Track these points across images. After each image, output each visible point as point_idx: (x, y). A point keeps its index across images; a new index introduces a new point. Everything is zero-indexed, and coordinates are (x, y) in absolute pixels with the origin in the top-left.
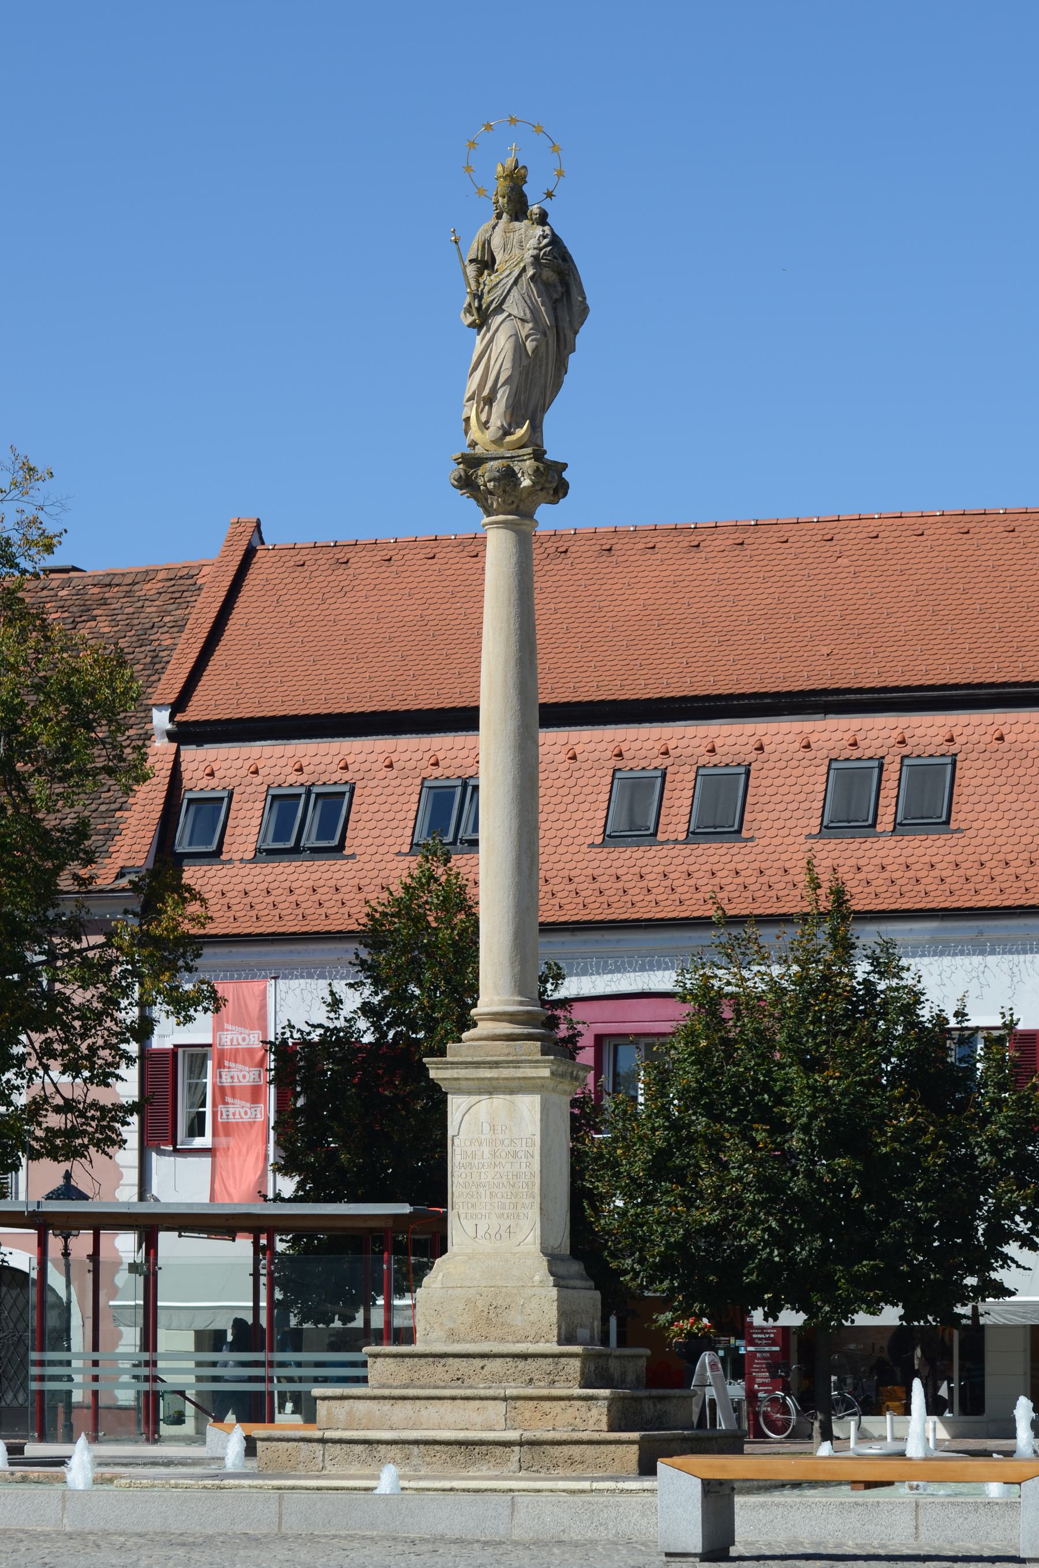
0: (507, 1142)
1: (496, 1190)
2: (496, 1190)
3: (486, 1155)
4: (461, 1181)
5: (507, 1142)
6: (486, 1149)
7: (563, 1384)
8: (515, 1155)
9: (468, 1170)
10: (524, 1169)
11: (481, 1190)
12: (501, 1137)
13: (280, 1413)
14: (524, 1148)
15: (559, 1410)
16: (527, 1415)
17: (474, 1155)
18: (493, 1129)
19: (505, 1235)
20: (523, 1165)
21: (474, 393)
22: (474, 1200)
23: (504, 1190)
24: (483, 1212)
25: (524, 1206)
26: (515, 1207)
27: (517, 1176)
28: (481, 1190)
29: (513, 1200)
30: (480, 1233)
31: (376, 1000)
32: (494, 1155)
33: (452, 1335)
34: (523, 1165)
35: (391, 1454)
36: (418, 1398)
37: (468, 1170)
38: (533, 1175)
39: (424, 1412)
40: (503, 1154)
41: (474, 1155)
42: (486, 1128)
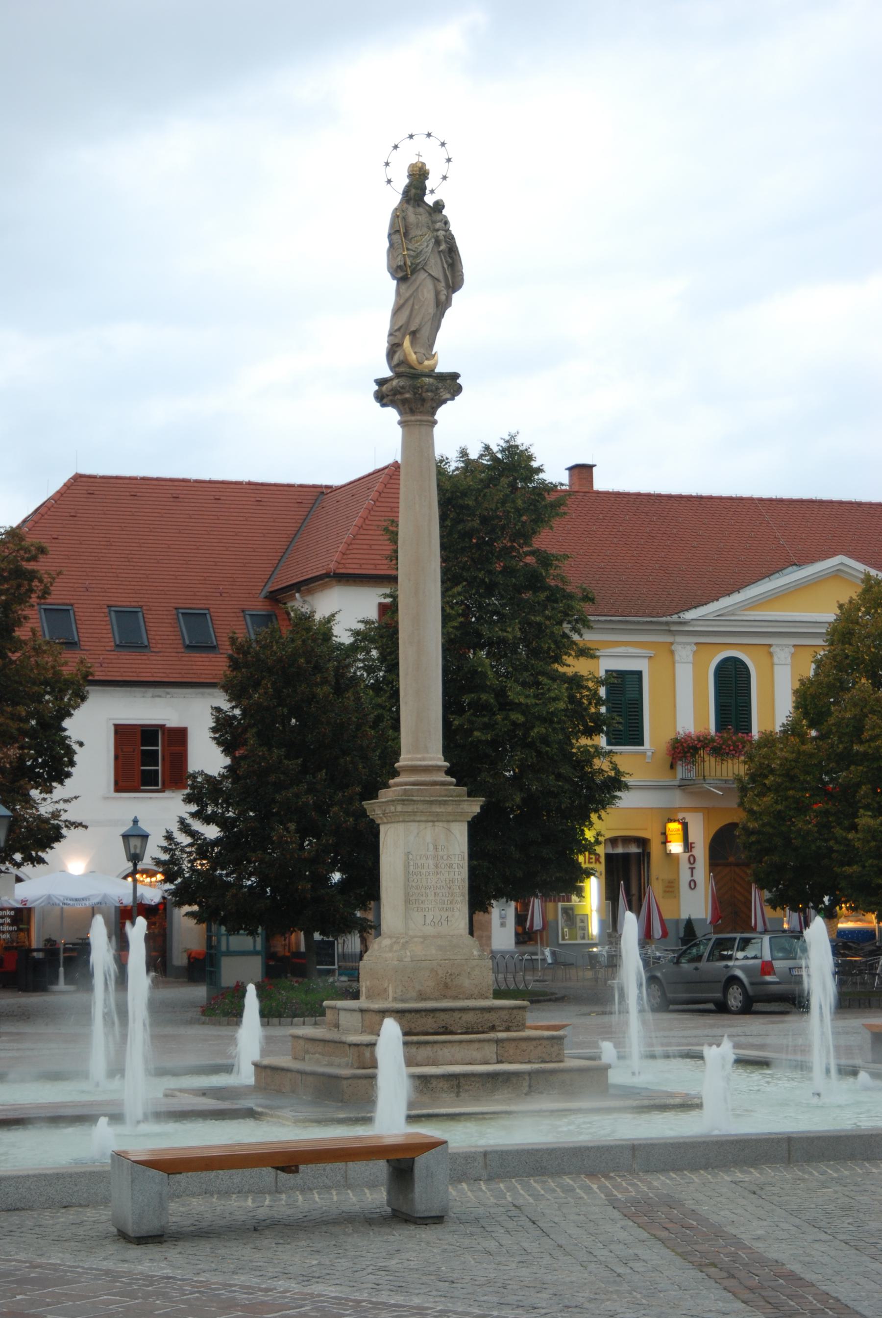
0: (445, 857)
1: (438, 891)
2: (438, 891)
3: (432, 866)
4: (414, 884)
5: (445, 857)
6: (431, 862)
7: (515, 1029)
8: (451, 866)
9: (419, 877)
10: (456, 876)
11: (428, 891)
12: (441, 853)
13: (600, 1058)
14: (457, 861)
15: (532, 1048)
16: (511, 1052)
17: (423, 866)
18: (436, 848)
19: (445, 923)
20: (456, 873)
21: (401, 327)
22: (423, 898)
23: (443, 891)
24: (430, 906)
25: (456, 902)
26: (451, 903)
27: (452, 881)
28: (428, 891)
29: (450, 898)
30: (428, 921)
31: (602, 741)
32: (437, 867)
33: (422, 996)
34: (456, 873)
35: (441, 1085)
36: (435, 1042)
37: (419, 877)
38: (463, 880)
39: (440, 1053)
40: (443, 866)
41: (423, 866)
42: (431, 847)
